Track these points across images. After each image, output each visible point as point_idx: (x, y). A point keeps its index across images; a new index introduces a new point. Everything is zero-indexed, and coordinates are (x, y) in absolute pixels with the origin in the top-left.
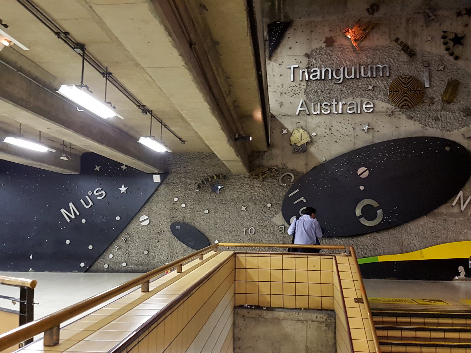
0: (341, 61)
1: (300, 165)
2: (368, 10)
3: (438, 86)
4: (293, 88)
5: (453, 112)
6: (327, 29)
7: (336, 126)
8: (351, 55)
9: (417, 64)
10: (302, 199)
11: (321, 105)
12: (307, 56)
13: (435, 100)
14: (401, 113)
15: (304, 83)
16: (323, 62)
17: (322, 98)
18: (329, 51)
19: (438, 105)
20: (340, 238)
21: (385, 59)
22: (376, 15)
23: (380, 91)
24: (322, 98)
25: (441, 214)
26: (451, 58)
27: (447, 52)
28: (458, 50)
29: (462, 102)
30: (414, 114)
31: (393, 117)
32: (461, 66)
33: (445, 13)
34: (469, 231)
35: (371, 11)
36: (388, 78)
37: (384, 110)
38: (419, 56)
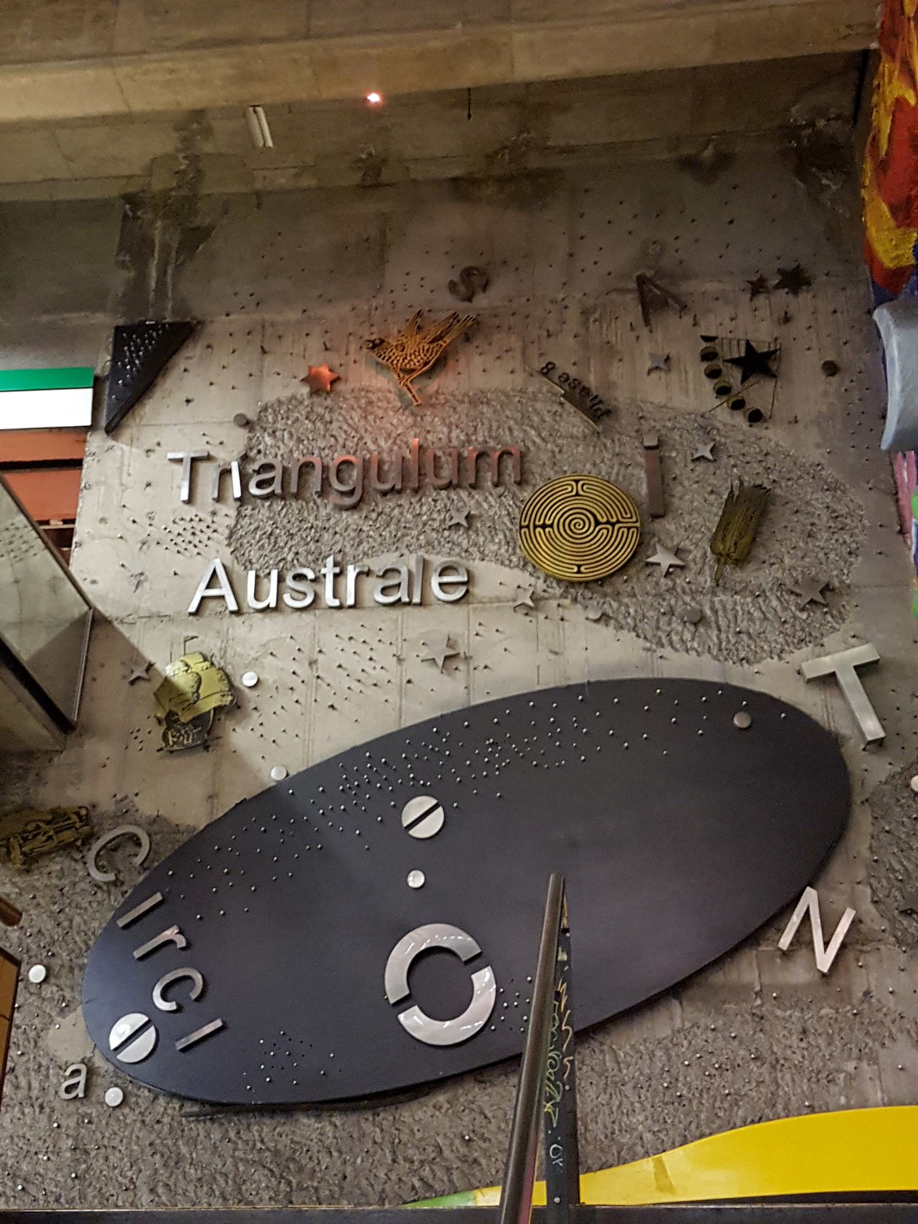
0: (361, 438)
1: (185, 797)
2: (452, 286)
3: (698, 510)
4: (188, 526)
5: (759, 594)
6: (315, 343)
7: (335, 651)
8: (395, 421)
9: (622, 444)
10: (171, 933)
11: (281, 579)
12: (246, 423)
13: (691, 557)
14: (567, 602)
15: (229, 510)
16: (299, 440)
17: (289, 558)
18: (320, 410)
19: (699, 573)
20: (325, 1115)
21: (510, 429)
22: (482, 301)
23: (493, 530)
24: (289, 558)
25: (740, 992)
26: (740, 420)
27: (724, 398)
28: (759, 394)
29: (787, 561)
30: (615, 605)
31: (541, 617)
32: (777, 445)
33: (712, 287)
34: (864, 1065)
35: (462, 289)
36: (522, 490)
37: (506, 592)
38: (626, 420)
